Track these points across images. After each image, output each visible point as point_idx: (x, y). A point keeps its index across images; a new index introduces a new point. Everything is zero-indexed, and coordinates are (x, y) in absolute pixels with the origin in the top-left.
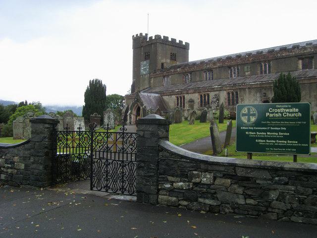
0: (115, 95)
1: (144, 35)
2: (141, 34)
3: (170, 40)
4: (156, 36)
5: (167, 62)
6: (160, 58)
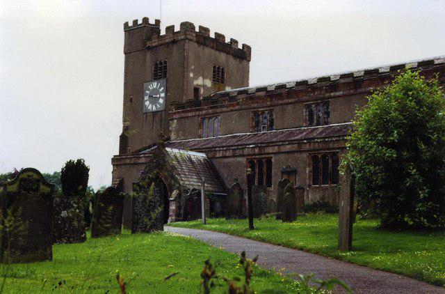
0: (25, 171)
1: (152, 22)
2: (146, 20)
3: (212, 35)
4: (183, 25)
5: (204, 83)
6: (191, 75)
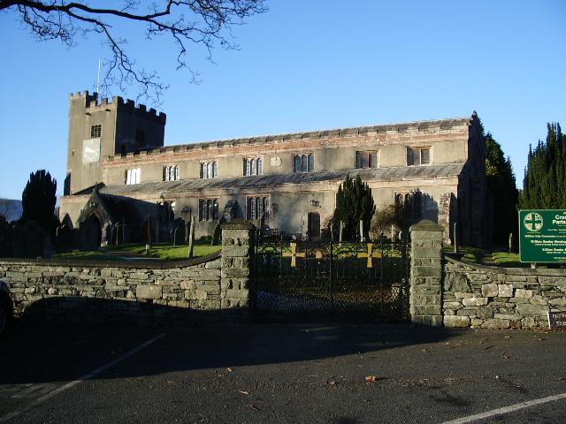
1: (91, 94)
